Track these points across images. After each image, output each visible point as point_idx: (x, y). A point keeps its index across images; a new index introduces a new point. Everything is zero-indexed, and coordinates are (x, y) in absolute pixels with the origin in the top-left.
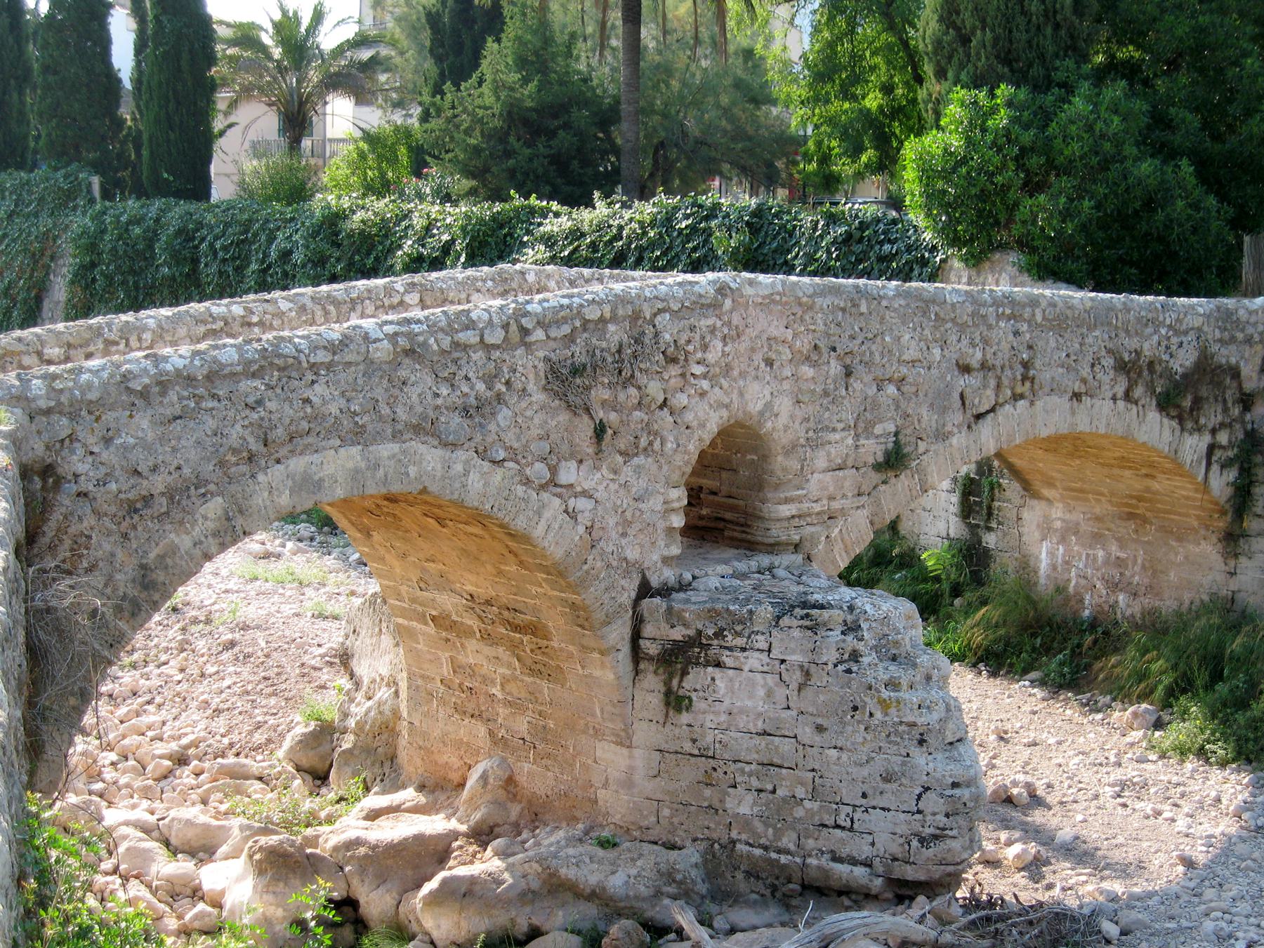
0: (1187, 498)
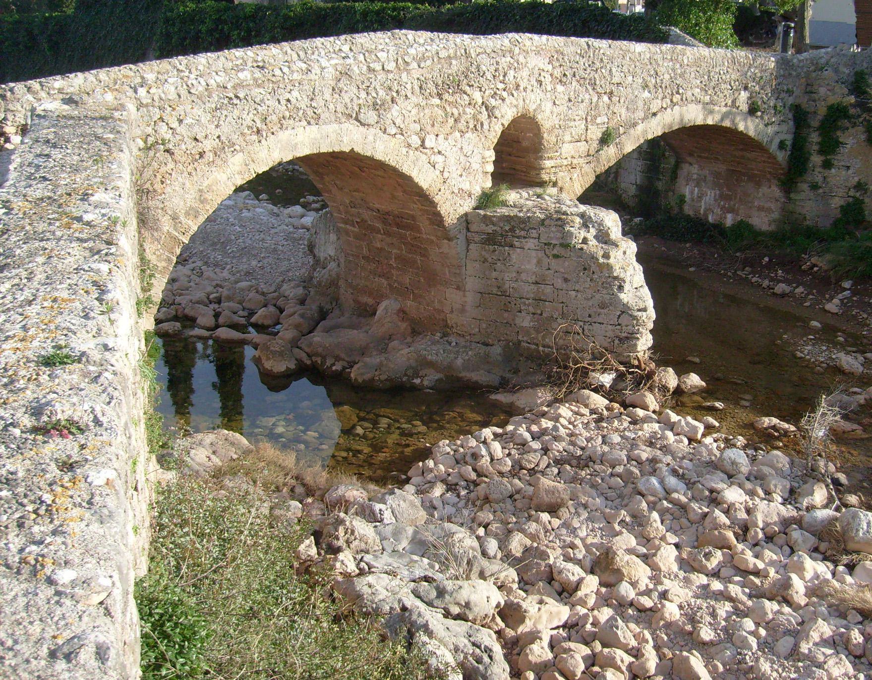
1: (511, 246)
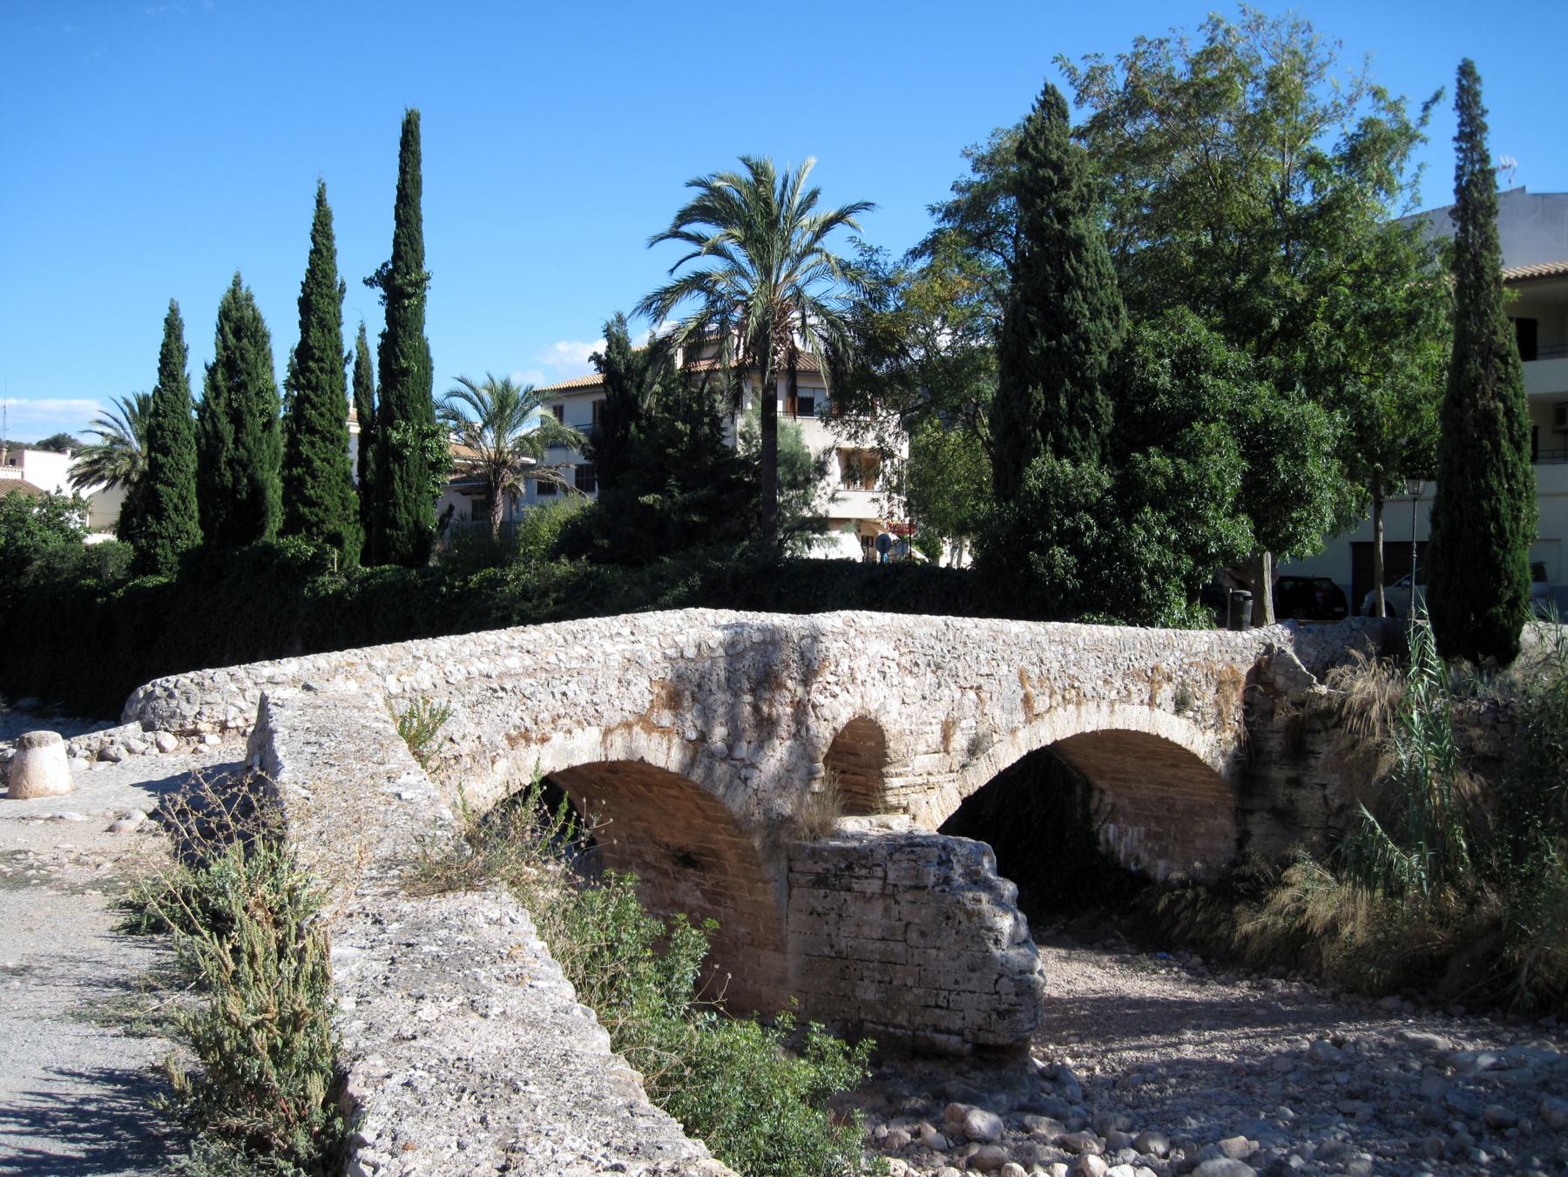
0: (1203, 782)
1: (849, 890)
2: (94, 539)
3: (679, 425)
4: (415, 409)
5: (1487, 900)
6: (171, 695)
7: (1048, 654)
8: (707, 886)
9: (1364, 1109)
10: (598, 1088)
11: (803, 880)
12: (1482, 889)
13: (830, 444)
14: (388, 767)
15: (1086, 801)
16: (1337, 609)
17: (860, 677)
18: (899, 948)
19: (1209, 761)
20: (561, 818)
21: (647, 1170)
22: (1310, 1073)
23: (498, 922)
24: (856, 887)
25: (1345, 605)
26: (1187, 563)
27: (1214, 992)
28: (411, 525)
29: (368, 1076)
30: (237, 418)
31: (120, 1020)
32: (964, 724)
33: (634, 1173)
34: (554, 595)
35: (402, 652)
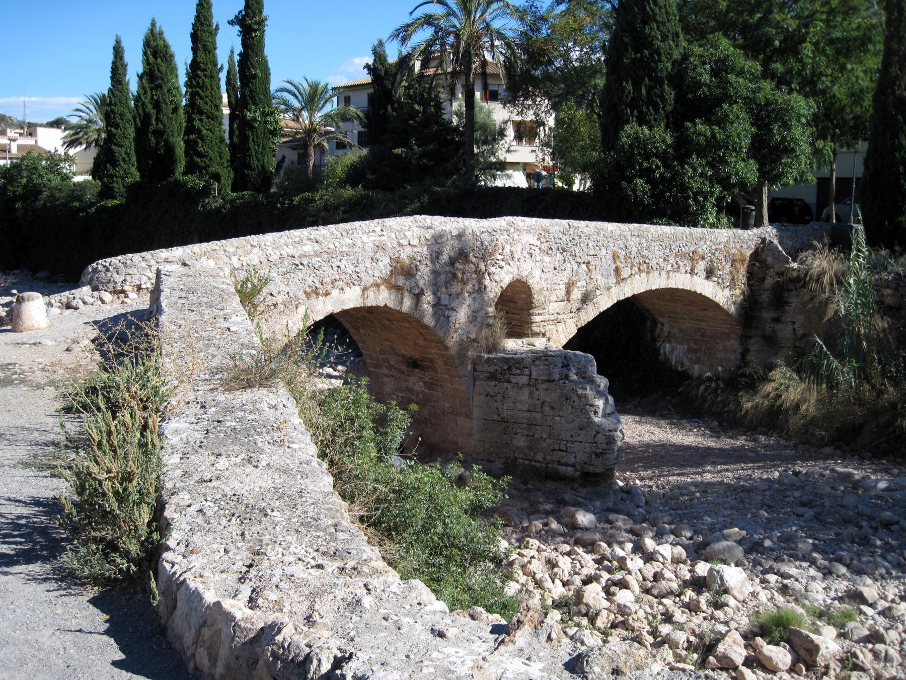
0: (722, 319)
1: (509, 382)
2: (78, 179)
3: (416, 106)
4: (260, 98)
5: (888, 391)
6: (108, 270)
7: (630, 243)
8: (427, 380)
9: (809, 513)
10: (317, 514)
11: (482, 376)
12: (885, 385)
13: (506, 118)
14: (225, 311)
15: (653, 330)
16: (807, 218)
17: (516, 256)
18: (538, 416)
19: (726, 307)
20: (319, 345)
21: (338, 568)
22: (778, 490)
23: (275, 407)
24: (513, 380)
25: (812, 216)
26: (718, 189)
27: (726, 443)
28: (260, 168)
29: (178, 505)
30: (157, 106)
31: (50, 467)
32: (579, 284)
33: (330, 570)
34: (343, 208)
35: (244, 243)
